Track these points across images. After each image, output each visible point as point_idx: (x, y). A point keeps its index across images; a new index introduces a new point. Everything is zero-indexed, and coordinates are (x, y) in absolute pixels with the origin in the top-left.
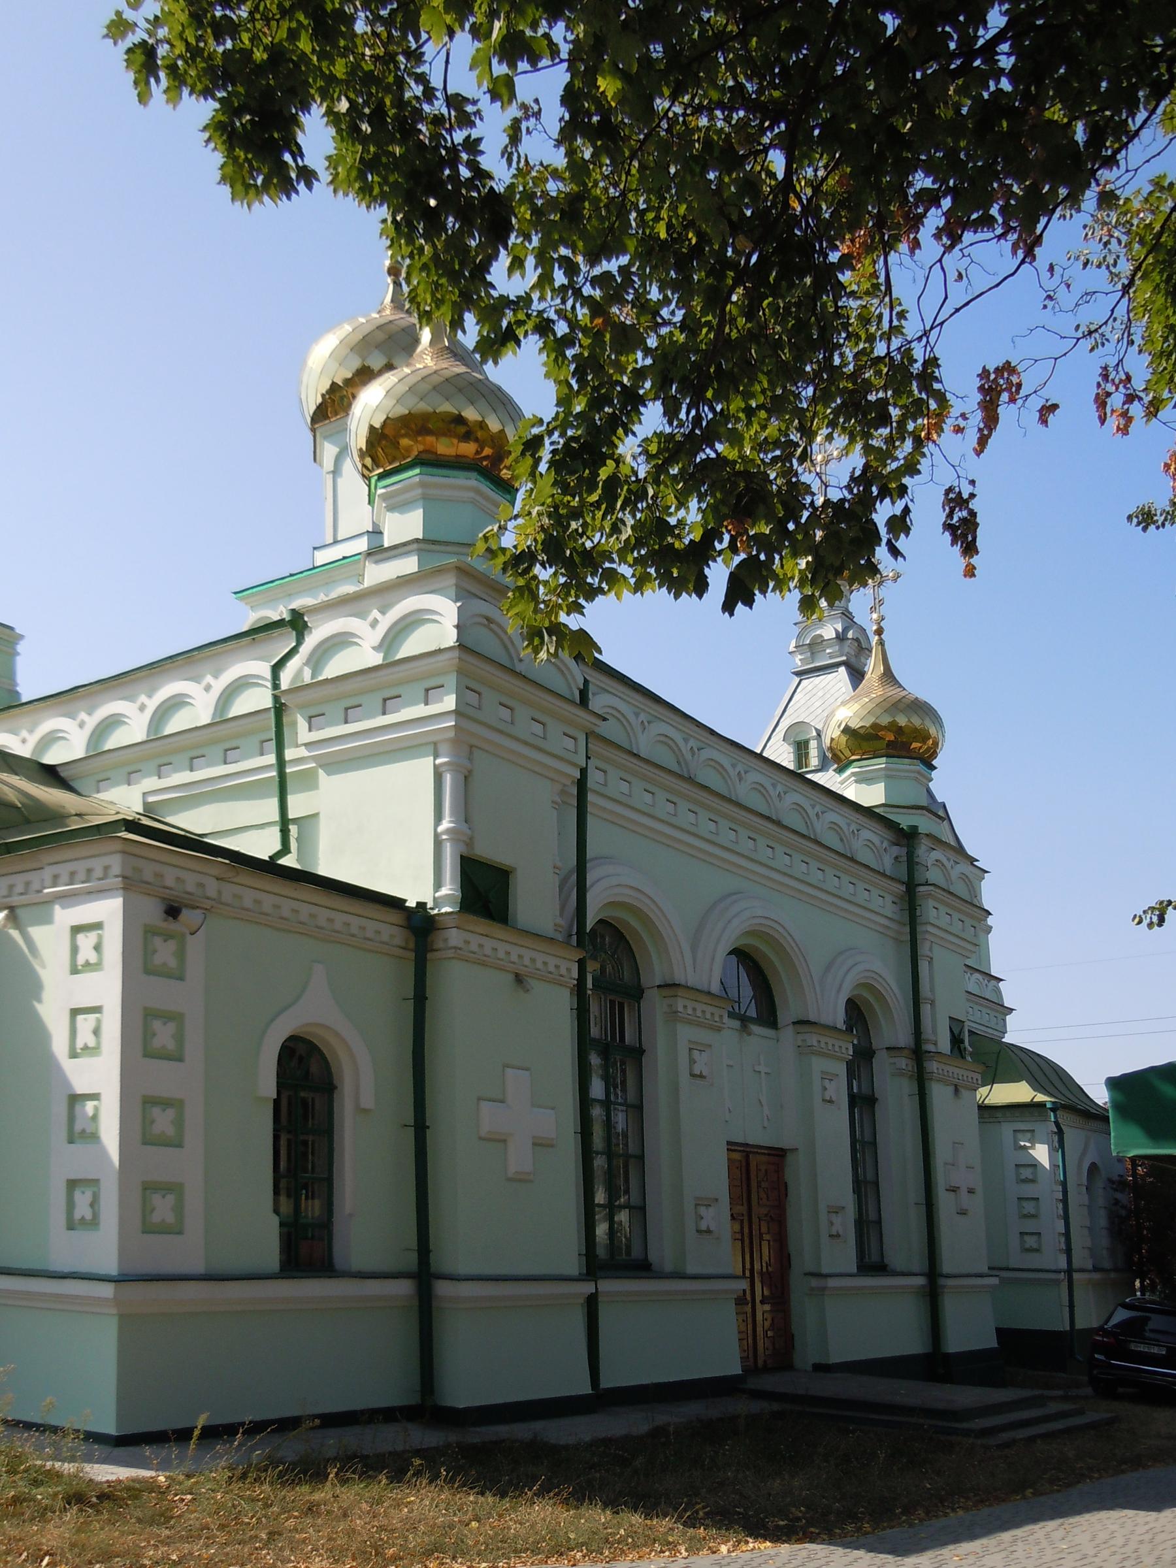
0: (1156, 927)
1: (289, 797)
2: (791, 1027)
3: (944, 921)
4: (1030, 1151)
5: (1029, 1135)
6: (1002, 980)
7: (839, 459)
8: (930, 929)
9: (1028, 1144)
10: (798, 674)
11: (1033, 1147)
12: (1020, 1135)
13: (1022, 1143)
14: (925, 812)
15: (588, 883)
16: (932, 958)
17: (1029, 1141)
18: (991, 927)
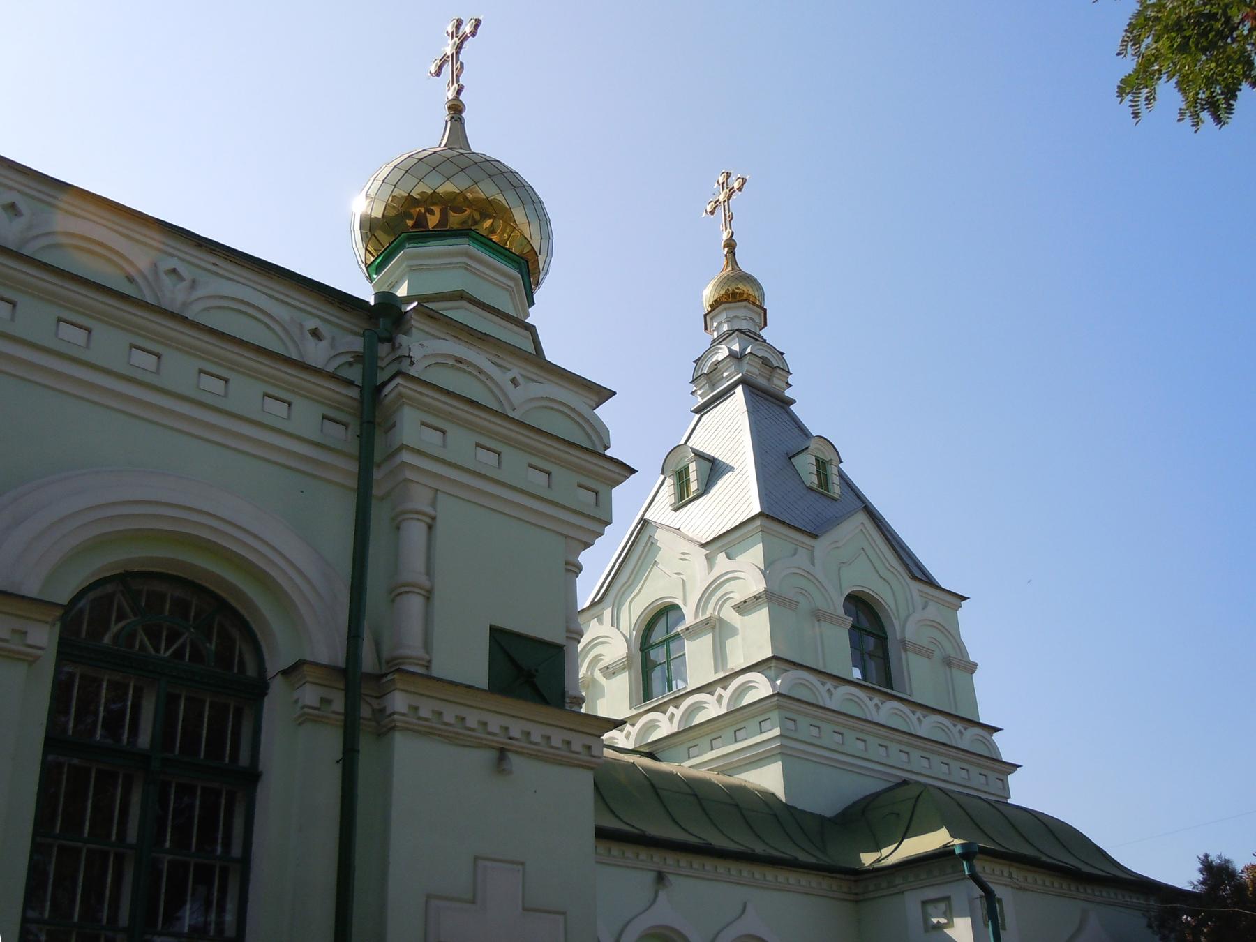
0: (471, 38)
1: (599, 715)
2: (279, 677)
3: (430, 439)
4: (947, 931)
5: (942, 906)
6: (997, 730)
7: (740, 189)
8: (406, 457)
9: (943, 921)
10: (697, 411)
11: (950, 924)
12: (930, 908)
13: (935, 920)
14: (464, 303)
15: (894, 784)
16: (434, 518)
17: (945, 915)
18: (976, 665)
